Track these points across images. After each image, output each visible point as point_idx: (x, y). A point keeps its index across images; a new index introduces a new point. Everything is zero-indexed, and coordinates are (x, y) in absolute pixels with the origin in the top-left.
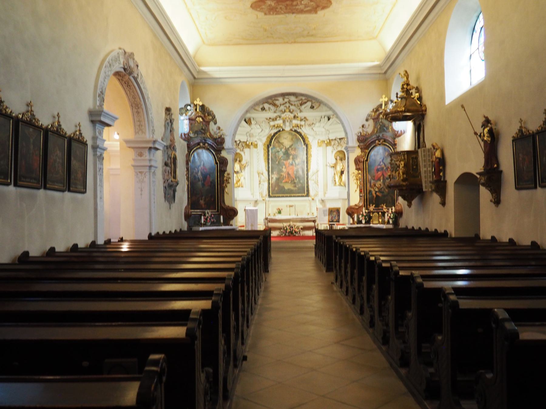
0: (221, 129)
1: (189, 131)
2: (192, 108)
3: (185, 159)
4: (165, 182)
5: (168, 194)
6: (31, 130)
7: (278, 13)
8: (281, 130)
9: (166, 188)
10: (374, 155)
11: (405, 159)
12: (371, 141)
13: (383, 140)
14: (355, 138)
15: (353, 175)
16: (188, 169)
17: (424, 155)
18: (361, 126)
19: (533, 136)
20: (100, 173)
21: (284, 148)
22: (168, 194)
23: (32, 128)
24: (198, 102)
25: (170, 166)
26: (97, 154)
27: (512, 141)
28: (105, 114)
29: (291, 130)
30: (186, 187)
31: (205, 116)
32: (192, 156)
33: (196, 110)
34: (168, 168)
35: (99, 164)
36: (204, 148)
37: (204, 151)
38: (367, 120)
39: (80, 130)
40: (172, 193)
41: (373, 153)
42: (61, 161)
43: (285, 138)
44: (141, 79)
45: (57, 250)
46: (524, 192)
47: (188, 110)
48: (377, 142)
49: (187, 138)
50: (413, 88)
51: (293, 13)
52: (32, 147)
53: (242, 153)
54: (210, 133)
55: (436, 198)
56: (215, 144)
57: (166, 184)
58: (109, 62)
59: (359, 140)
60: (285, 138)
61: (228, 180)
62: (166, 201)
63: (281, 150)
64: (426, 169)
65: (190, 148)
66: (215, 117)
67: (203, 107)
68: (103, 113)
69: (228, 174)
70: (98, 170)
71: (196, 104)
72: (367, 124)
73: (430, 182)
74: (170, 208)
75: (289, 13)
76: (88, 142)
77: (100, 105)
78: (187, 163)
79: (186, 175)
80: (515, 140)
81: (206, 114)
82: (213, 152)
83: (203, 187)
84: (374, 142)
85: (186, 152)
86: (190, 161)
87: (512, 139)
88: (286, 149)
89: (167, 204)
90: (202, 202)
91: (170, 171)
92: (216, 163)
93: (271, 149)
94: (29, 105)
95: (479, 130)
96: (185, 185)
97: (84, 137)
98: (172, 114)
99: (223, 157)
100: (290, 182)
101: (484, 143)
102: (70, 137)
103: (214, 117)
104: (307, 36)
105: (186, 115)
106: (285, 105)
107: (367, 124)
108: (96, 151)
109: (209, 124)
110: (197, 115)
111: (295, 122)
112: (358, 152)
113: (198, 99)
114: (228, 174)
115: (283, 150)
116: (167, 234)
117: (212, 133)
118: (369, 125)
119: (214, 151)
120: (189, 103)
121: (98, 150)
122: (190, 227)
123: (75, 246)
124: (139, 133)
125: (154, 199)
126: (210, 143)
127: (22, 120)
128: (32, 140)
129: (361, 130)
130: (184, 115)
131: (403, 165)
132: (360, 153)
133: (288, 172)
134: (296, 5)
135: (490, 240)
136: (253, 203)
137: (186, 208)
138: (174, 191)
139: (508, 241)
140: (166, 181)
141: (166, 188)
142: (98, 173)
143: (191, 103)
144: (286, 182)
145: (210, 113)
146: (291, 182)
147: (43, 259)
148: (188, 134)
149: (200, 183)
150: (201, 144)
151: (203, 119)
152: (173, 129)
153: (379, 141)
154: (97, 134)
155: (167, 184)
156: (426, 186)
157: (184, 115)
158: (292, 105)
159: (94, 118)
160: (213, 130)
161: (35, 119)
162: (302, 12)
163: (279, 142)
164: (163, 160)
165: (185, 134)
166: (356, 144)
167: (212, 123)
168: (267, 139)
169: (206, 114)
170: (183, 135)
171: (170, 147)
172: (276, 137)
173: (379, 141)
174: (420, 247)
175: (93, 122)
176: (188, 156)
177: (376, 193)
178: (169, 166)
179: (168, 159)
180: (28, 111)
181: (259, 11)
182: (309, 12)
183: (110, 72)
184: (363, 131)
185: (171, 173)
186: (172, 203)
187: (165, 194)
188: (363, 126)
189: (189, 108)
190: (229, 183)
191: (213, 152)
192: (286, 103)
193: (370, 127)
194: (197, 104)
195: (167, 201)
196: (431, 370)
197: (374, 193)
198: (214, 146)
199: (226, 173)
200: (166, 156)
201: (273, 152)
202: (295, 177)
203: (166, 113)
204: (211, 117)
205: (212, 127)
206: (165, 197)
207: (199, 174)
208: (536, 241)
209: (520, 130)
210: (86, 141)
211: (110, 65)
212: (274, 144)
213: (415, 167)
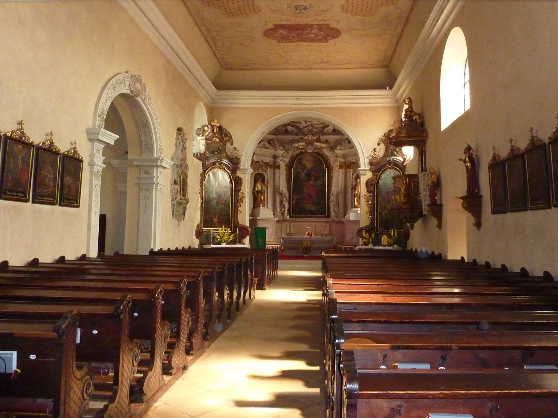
0: (237, 150)
1: (205, 151)
2: (209, 129)
3: (198, 178)
4: (173, 200)
5: (177, 212)
6: (20, 147)
7: (291, 41)
8: (304, 151)
9: (174, 205)
10: (385, 178)
11: (406, 182)
12: (382, 164)
13: (393, 164)
14: (367, 161)
15: (364, 197)
16: (202, 187)
17: (424, 179)
18: (373, 150)
19: (503, 162)
20: (96, 189)
21: (306, 169)
22: (177, 212)
23: (21, 145)
24: (216, 123)
25: (180, 184)
26: (93, 171)
27: (488, 167)
28: (103, 133)
29: (313, 152)
30: (200, 205)
31: (222, 137)
32: (208, 175)
33: (213, 131)
34: (177, 187)
35: (95, 181)
36: (220, 168)
37: (219, 170)
38: (379, 144)
39: (75, 148)
40: (181, 210)
41: (383, 176)
42: (52, 176)
44: (149, 101)
45: (40, 261)
46: (498, 216)
47: (204, 130)
48: (388, 165)
49: (200, 157)
50: (416, 114)
51: (305, 42)
52: (21, 162)
53: (265, 174)
54: (226, 153)
55: (434, 221)
56: (231, 164)
57: (175, 202)
58: (112, 85)
59: (371, 164)
61: (243, 199)
62: (174, 219)
63: (303, 172)
64: (425, 193)
65: (206, 169)
66: (232, 138)
67: (220, 128)
68: (101, 133)
69: (243, 193)
70: (94, 186)
71: (213, 125)
72: (378, 148)
73: (428, 205)
74: (178, 225)
75: (301, 41)
76: (83, 160)
77: (100, 124)
78: (202, 182)
79: (200, 193)
80: (491, 167)
81: (223, 135)
82: (228, 171)
83: (217, 206)
84: (384, 166)
85: (202, 171)
86: (205, 179)
87: (488, 165)
89: (175, 221)
90: (215, 220)
91: (179, 190)
92: (231, 183)
94: (20, 123)
95: (463, 157)
96: (198, 203)
97: (79, 154)
98: (184, 134)
99: (239, 177)
102: (63, 154)
103: (231, 138)
104: (322, 63)
105: (203, 136)
106: (307, 128)
107: (378, 148)
108: (93, 168)
109: (226, 145)
110: (215, 136)
111: (318, 144)
112: (369, 175)
113: (216, 121)
114: (243, 193)
115: (305, 171)
116: (180, 250)
117: (229, 154)
118: (380, 149)
119: (229, 170)
120: (207, 124)
121: (95, 167)
122: (201, 244)
123: (62, 259)
124: (147, 152)
125: (159, 215)
126: (225, 163)
127: (10, 138)
128: (20, 157)
129: (372, 154)
130: (201, 135)
131: (404, 188)
132: (372, 176)
134: (308, 34)
135: (484, 265)
137: (198, 226)
138: (184, 209)
139: (500, 267)
140: (175, 199)
141: (174, 205)
142: (93, 189)
143: (208, 123)
144: (307, 203)
145: (228, 135)
147: (26, 269)
148: (204, 154)
149: (214, 201)
150: (388, 165)
151: (219, 140)
152: (185, 148)
153: (390, 165)
154: (95, 151)
155: (176, 202)
156: (425, 210)
157: (201, 135)
158: (315, 128)
159: (92, 137)
160: (229, 150)
161: (25, 137)
162: (312, 40)
163: (301, 164)
164: (172, 178)
165: (201, 154)
166: (368, 167)
167: (228, 144)
168: (289, 160)
169: (223, 135)
170: (199, 154)
171: (181, 166)
173: (390, 165)
175: (90, 140)
176: (203, 175)
177: (386, 216)
178: (179, 185)
179: (177, 178)
180: (18, 130)
181: (271, 39)
182: (320, 40)
183: (113, 94)
184: (375, 154)
185: (180, 191)
186: (181, 220)
187: (173, 211)
188: (374, 150)
189: (206, 128)
190: (242, 202)
191: (228, 171)
192: (309, 125)
193: (381, 151)
194: (214, 125)
195: (176, 219)
197: (384, 214)
198: (229, 166)
199: (240, 192)
200: (176, 174)
203: (177, 133)
204: (227, 139)
205: (229, 147)
206: (173, 214)
207: (214, 193)
208: (506, 265)
209: (494, 158)
210: (82, 158)
211: (114, 87)
213: (416, 190)
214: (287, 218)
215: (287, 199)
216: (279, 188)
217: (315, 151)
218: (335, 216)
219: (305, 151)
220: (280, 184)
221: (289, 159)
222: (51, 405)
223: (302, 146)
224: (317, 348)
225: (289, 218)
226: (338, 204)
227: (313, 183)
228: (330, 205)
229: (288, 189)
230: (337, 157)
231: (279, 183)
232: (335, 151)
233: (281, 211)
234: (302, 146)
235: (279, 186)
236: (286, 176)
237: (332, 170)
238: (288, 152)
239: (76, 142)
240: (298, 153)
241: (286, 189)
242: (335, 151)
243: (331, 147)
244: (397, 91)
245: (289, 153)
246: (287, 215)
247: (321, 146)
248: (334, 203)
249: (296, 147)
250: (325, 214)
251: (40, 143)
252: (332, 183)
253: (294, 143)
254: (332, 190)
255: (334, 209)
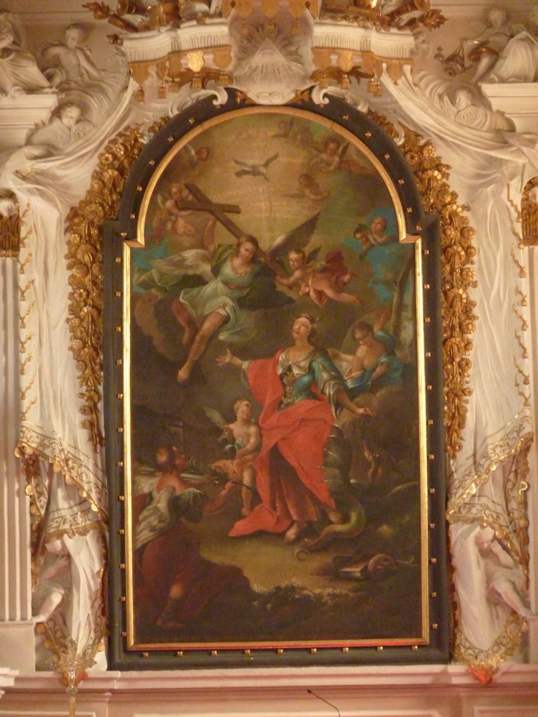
8: (222, 98)
21: (246, 247)
43: (254, 172)
60: (254, 172)
63: (216, 271)
88: (253, 260)
93: (133, 252)
100: (291, 534)
101: (315, 104)
133: (275, 451)
136: (88, 481)
146: (299, 538)
168: (97, 176)
172: (236, 118)
174: (201, 41)
196: (487, 476)
201: (147, 285)
202: (333, 494)
212: (155, 222)
214: (91, 671)
215: (83, 502)
216: (20, 416)
217: (318, 98)
218: (498, 644)
219: (232, 93)
220: (25, 381)
221: (92, 164)
222: (312, 19)
223: (205, 49)
224: (330, 454)
225: (111, 667)
226: (526, 541)
227: (311, 370)
228: (456, 550)
229: (91, 426)
230: (504, 144)
231: (19, 371)
232: (487, 89)
233: (35, 613)
234: (205, 49)
235: (19, 395)
236: (74, 310)
237: (468, 249)
238: (84, 109)
239: (85, 4)
240: (173, 113)
241: (78, 418)
242: (487, 89)
243: (452, 58)
244: (77, 149)
245: (95, 114)
246: (94, 646)
247: (365, 53)
248: (489, 533)
249: (159, 63)
250: (419, 635)
251: (117, 6)
252: (464, 365)
253: (133, 29)
254: (470, 419)
255: (489, 579)
